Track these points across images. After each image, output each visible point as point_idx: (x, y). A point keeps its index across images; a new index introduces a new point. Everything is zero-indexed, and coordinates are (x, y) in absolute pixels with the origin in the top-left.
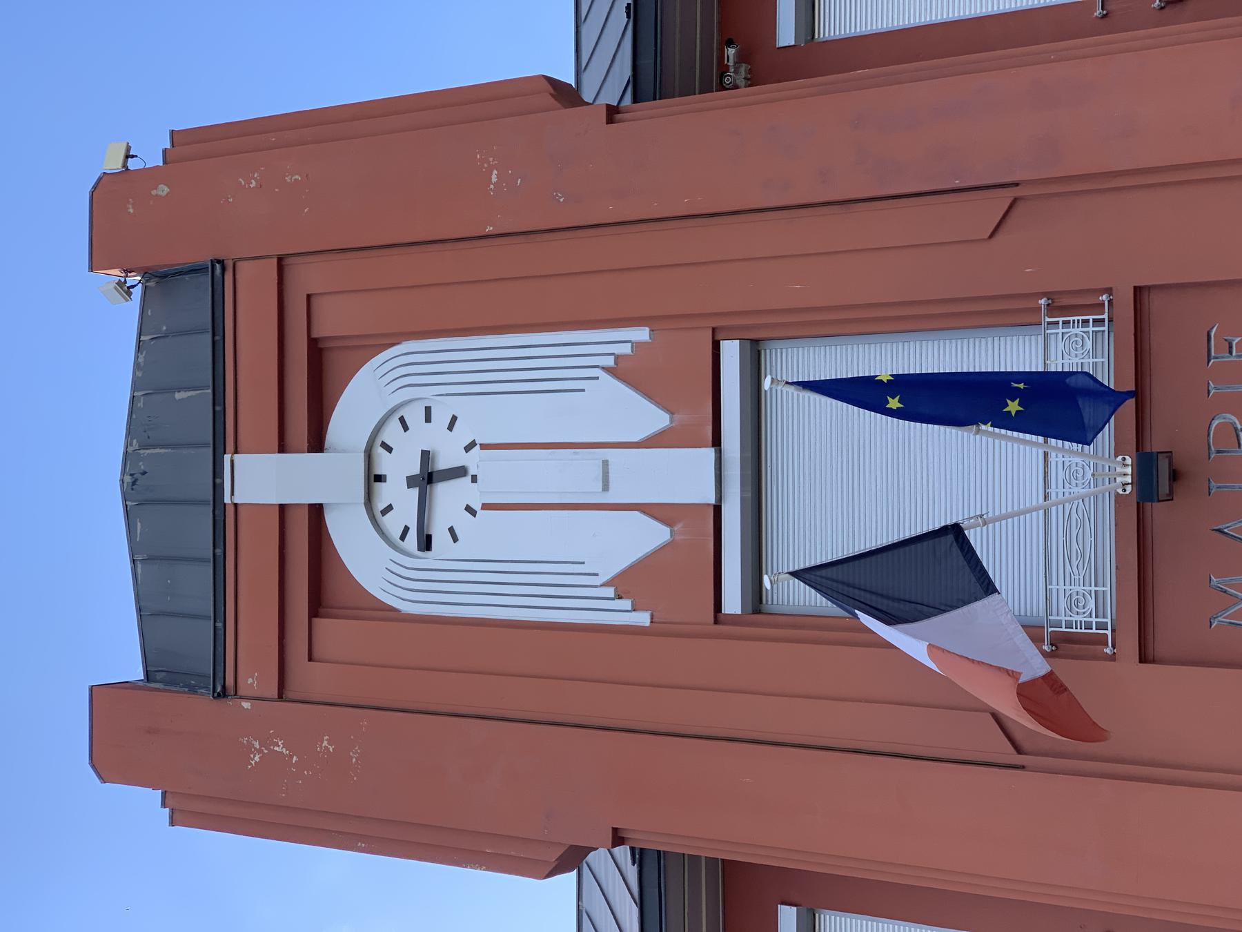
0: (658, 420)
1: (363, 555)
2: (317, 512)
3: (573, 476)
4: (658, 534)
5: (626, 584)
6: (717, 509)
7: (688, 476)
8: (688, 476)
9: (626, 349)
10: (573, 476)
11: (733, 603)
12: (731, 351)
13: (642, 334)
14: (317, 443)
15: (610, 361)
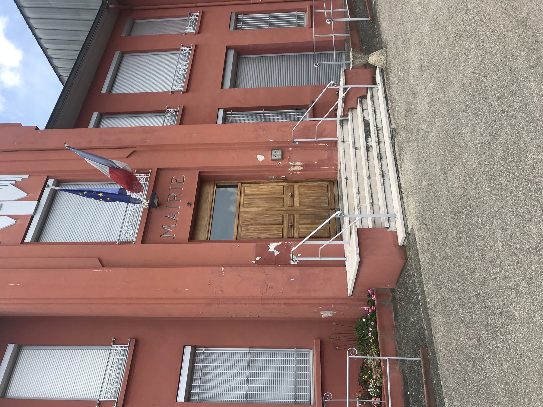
0: (23, 195)
6: (32, 217)
7: (28, 208)
9: (20, 180)
13: (26, 176)
15: (14, 182)
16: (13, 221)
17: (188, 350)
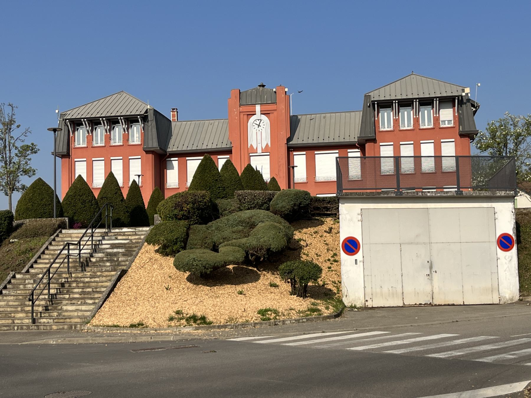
3: (259, 141)
4: (255, 148)
5: (251, 145)
7: (259, 151)
8: (259, 151)
10: (259, 141)
11: (251, 154)
12: (268, 154)
16: (255, 148)
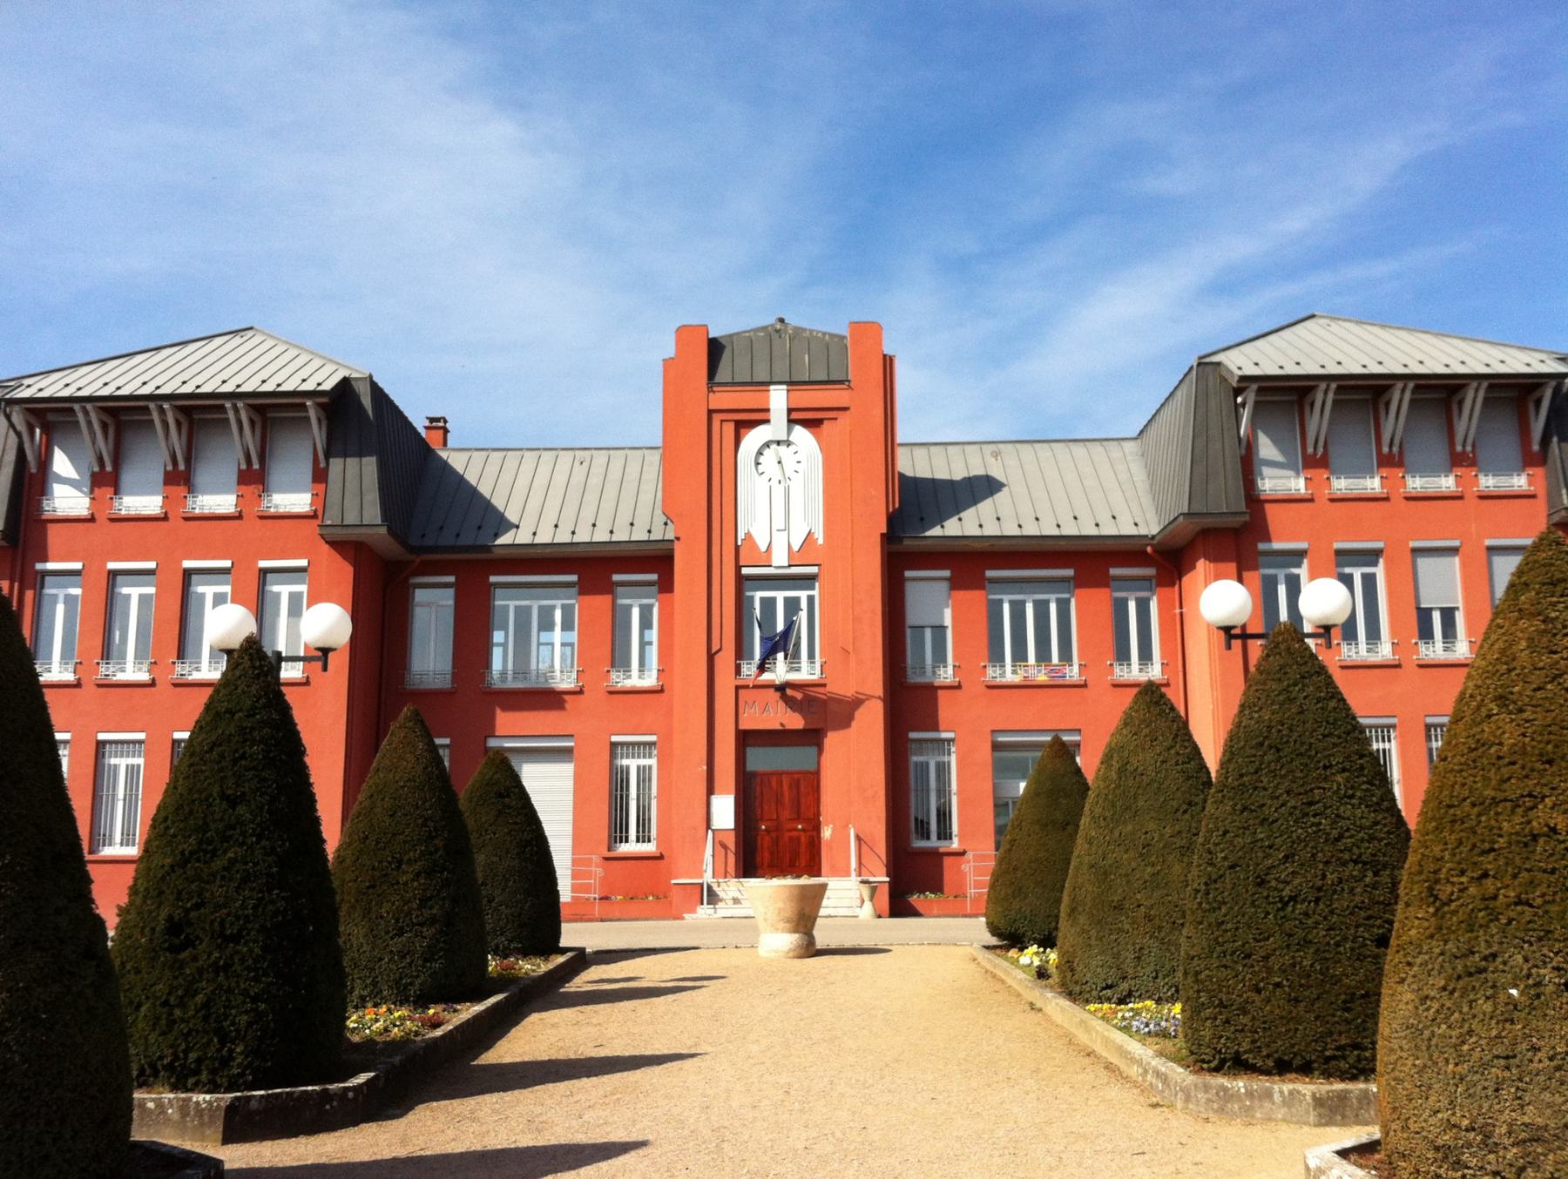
0: (796, 548)
1: (753, 439)
2: (767, 421)
5: (748, 536)
8: (780, 559)
10: (779, 522)
13: (821, 541)
14: (792, 422)
16: (763, 549)
17: (141, 736)
